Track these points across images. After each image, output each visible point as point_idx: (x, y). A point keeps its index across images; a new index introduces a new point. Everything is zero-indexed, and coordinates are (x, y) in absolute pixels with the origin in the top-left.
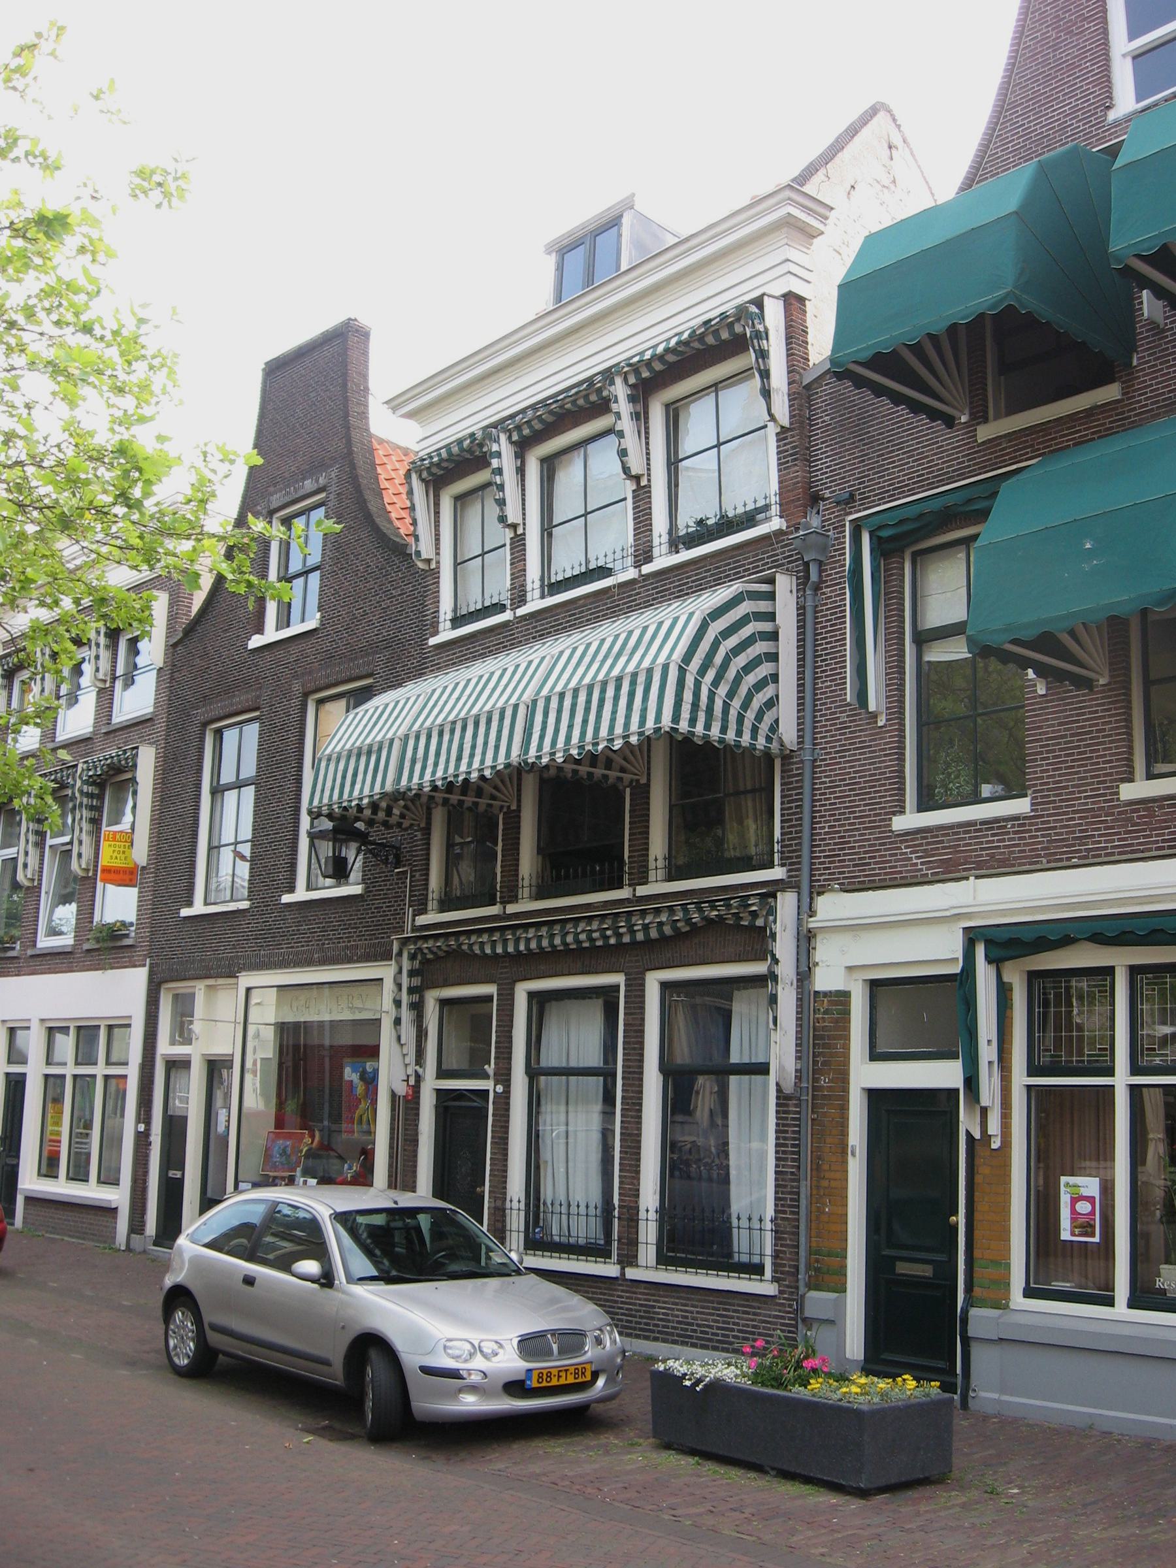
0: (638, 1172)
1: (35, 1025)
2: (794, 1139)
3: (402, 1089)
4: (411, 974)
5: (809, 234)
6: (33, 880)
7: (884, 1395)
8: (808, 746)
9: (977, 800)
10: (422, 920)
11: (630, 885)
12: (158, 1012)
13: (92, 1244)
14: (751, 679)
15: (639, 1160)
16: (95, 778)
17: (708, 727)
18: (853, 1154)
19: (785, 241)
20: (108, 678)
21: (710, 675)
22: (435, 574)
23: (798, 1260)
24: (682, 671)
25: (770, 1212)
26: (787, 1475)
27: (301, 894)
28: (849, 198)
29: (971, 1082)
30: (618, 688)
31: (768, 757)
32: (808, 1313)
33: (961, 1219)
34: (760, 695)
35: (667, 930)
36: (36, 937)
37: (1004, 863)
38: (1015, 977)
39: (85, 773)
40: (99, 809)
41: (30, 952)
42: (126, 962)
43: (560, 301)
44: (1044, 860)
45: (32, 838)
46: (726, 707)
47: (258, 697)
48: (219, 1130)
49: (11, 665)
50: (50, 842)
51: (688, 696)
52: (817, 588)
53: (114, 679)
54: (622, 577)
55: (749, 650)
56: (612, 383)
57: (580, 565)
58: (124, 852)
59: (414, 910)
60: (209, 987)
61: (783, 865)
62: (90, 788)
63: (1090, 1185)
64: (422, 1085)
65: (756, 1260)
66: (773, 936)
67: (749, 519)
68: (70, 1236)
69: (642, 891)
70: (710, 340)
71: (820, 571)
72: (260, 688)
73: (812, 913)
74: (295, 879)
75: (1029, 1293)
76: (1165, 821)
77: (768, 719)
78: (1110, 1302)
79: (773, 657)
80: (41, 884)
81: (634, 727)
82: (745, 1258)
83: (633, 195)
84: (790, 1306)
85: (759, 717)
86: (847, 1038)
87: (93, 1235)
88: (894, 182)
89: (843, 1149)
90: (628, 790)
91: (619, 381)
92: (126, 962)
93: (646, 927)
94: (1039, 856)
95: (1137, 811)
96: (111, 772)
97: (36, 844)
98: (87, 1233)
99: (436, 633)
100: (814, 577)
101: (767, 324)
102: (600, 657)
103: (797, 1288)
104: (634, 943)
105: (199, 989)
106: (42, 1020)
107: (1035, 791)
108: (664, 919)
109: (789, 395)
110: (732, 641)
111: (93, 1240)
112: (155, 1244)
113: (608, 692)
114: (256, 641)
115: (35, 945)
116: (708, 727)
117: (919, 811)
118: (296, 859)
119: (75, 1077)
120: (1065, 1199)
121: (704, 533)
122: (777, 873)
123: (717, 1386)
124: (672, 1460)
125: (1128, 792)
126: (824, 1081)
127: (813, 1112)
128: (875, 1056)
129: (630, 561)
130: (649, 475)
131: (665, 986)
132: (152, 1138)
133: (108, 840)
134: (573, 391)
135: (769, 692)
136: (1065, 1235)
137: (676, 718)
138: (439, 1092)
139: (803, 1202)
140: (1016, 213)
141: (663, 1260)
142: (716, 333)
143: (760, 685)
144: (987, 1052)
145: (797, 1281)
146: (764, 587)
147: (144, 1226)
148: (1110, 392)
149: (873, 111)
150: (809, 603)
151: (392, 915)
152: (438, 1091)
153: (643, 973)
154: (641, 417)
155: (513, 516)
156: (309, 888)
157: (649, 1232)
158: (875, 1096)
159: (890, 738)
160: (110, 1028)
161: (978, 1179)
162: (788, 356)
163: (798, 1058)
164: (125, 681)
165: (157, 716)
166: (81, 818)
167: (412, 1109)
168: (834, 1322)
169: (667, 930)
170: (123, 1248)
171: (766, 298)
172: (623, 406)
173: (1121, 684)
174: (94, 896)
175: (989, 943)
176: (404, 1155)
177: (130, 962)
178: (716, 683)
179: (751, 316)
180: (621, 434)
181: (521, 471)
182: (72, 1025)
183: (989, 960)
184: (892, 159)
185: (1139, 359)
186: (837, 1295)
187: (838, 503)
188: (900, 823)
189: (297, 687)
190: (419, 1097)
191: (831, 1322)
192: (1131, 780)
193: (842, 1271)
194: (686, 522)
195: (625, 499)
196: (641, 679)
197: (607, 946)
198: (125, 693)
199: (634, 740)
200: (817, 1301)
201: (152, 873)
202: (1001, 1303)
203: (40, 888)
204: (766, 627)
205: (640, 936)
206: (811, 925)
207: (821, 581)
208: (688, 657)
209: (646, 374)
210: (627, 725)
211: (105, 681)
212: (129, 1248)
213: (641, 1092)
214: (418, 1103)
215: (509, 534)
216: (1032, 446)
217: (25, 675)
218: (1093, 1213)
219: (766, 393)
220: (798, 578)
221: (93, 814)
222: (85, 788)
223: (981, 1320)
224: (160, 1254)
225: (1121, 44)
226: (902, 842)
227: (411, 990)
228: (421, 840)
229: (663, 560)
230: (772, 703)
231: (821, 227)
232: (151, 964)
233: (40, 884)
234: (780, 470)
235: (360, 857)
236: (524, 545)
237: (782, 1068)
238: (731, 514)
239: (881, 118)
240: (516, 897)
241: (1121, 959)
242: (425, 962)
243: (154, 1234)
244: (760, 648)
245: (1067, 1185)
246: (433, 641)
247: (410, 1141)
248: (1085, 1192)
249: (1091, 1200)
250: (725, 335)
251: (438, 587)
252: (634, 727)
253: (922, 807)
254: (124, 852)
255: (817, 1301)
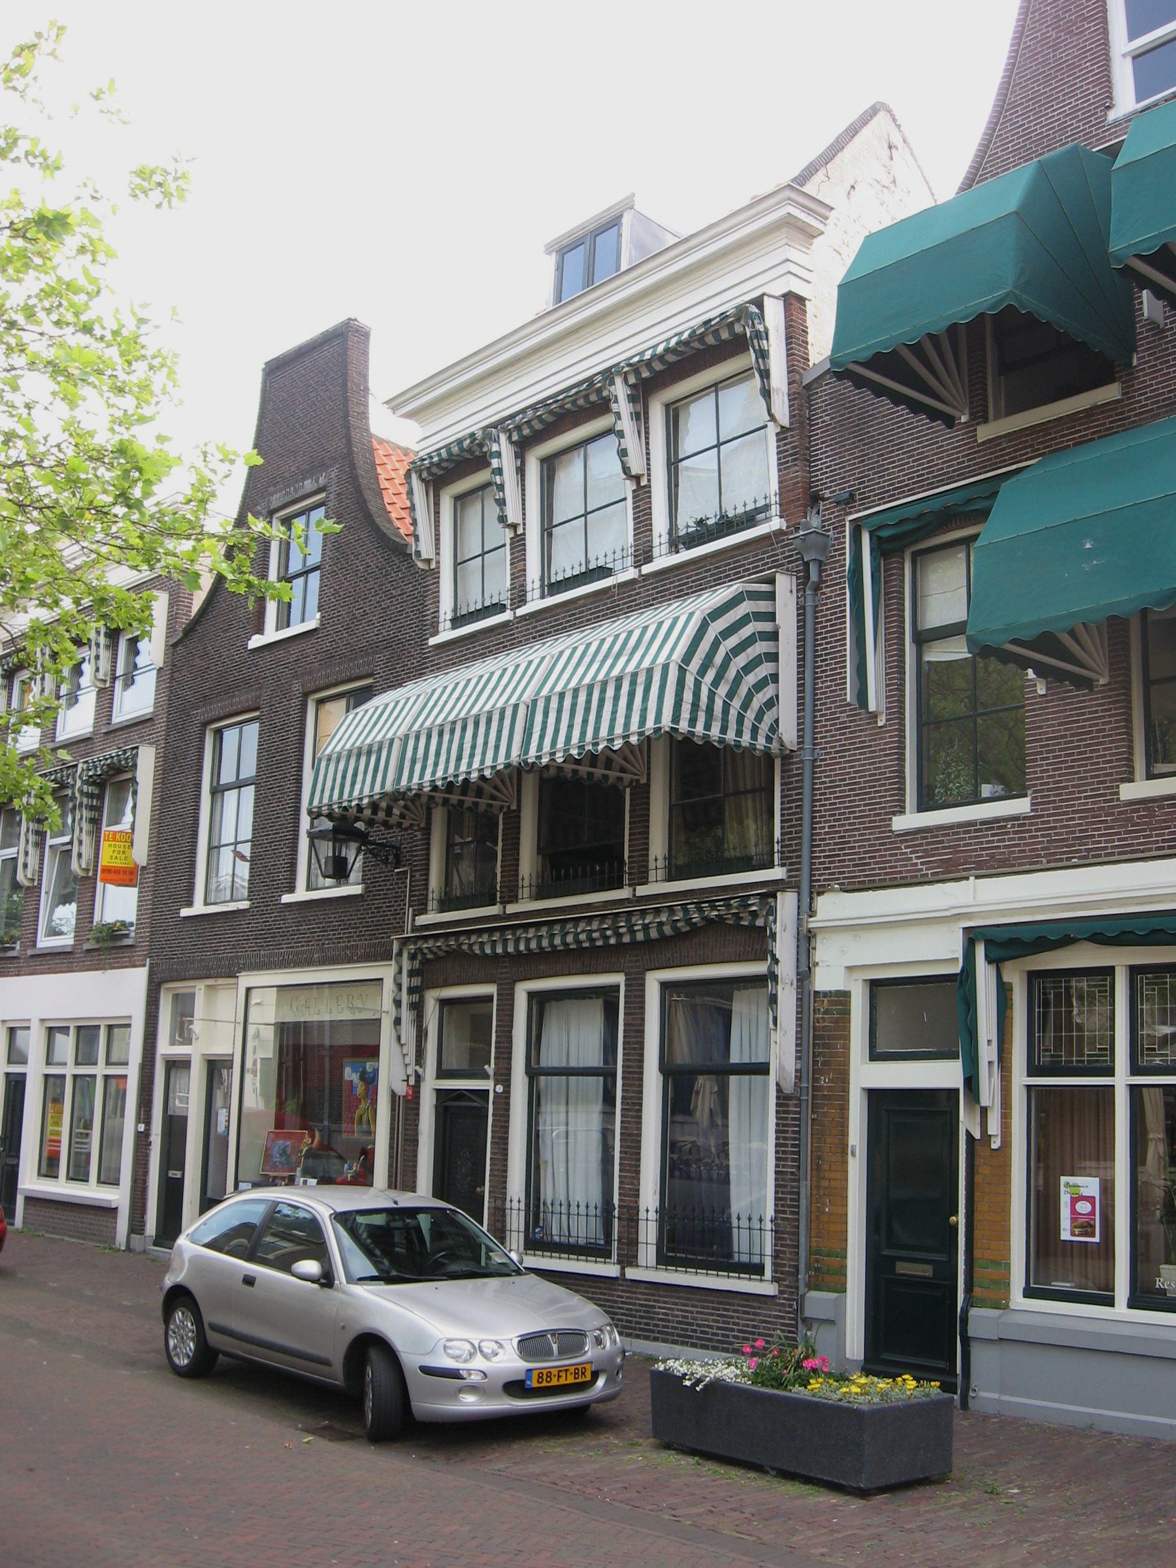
0: (638, 1172)
1: (35, 1025)
2: (794, 1139)
3: (402, 1089)
4: (411, 974)
5: (809, 234)
6: (33, 880)
7: (884, 1395)
8: (808, 746)
9: (977, 800)
10: (422, 920)
11: (630, 885)
12: (158, 1012)
13: (92, 1244)
14: (751, 679)
15: (639, 1160)
16: (95, 778)
17: (708, 727)
18: (853, 1154)
19: (785, 241)
20: (108, 678)
21: (710, 675)
22: (435, 574)
23: (798, 1260)
24: (682, 671)
25: (770, 1212)
26: (787, 1475)
27: (301, 894)
28: (849, 198)
29: (971, 1082)
30: (618, 688)
31: (768, 757)
32: (808, 1313)
33: (961, 1219)
34: (760, 695)
35: (667, 930)
36: (36, 937)
37: (1004, 863)
38: (1015, 977)
39: (85, 773)
40: (99, 809)
41: (30, 952)
42: (126, 962)
43: (560, 301)
44: (1044, 860)
45: (32, 838)
46: (726, 707)
47: (258, 697)
48: (219, 1130)
49: (11, 665)
50: (50, 842)
51: (688, 696)
52: (817, 588)
53: (114, 679)
54: (622, 577)
55: (749, 650)
56: (612, 383)
57: (580, 565)
58: (124, 852)
59: (414, 910)
60: (209, 987)
61: (783, 865)
62: (90, 788)
63: (1090, 1185)
64: (422, 1085)
65: (756, 1260)
66: (773, 936)
67: (749, 519)
68: (70, 1236)
69: (642, 891)
70: (710, 340)
71: (820, 571)
72: (260, 688)
73: (812, 913)
74: (295, 879)
75: (1029, 1293)
76: (1165, 821)
77: (768, 719)
78: (1110, 1302)
79: (773, 657)
80: (41, 884)
81: (634, 727)
82: (745, 1258)
83: (633, 195)
84: (790, 1306)
85: (759, 717)
86: (847, 1038)
87: (93, 1235)
88: (894, 182)
89: (843, 1149)
90: (628, 790)
91: (619, 381)
92: (126, 962)
93: (646, 927)
94: (1039, 856)
95: (1137, 811)
96: (111, 772)
97: (36, 844)
98: (87, 1233)
99: (436, 633)
100: (814, 577)
101: (767, 324)
102: (600, 657)
103: (797, 1288)
104: (634, 943)
105: (199, 989)
106: (42, 1020)
107: (1035, 791)
108: (664, 919)
109: (789, 395)
110: (732, 641)
111: (93, 1240)
112: (155, 1244)
113: (608, 692)
114: (256, 641)
115: (35, 945)
116: (708, 727)
117: (919, 811)
118: (296, 859)
119: (75, 1077)
120: (1065, 1199)
121: (704, 533)
122: (777, 873)
123: (717, 1386)
124: (672, 1460)
125: (1128, 792)
126: (824, 1081)
127: (813, 1112)
128: (875, 1056)
129: (630, 561)
130: (649, 475)
131: (665, 986)
132: (152, 1138)
133: (108, 840)
134: (573, 391)
135: (769, 692)
136: (1065, 1235)
137: (676, 718)
138: (439, 1092)
139: (803, 1202)
140: (1016, 213)
141: (663, 1260)
142: (716, 333)
143: (760, 685)
144: (987, 1052)
145: (797, 1281)
146: (764, 587)
147: (144, 1226)
148: (1110, 392)
149: (873, 111)
150: (809, 603)
151: (392, 915)
152: (438, 1091)
153: (643, 973)
154: (641, 417)
155: (513, 516)
156: (309, 888)
157: (649, 1232)
158: (875, 1096)
159: (890, 738)
160: (110, 1028)
161: (978, 1179)
162: (788, 356)
163: (798, 1058)
164: (125, 681)
165: (157, 716)
166: (81, 818)
167: (412, 1109)
168: (834, 1322)
169: (667, 930)
170: (123, 1248)
171: (766, 298)
172: (623, 406)
173: (1121, 684)
174: (94, 896)
175: (989, 943)
176: (404, 1155)
177: (130, 962)
178: (716, 683)
179: (751, 316)
180: (621, 434)
181: (521, 471)
182: (72, 1025)
183: (989, 960)
184: (892, 159)
185: (1139, 359)
186: (837, 1295)
187: (838, 503)
188: (900, 823)
189: (297, 687)
190: (419, 1097)
191: (831, 1322)
192: (1131, 780)
193: (842, 1271)
194: (686, 522)
195: (625, 499)
196: (641, 679)
197: (607, 946)
198: (125, 693)
199: (634, 740)
200: (817, 1301)
201: (152, 873)
202: (1001, 1303)
203: (40, 888)
204: (766, 627)
205: (640, 936)
206: (811, 925)
207: (821, 581)
208: (688, 657)
209: (646, 374)
210: (627, 725)
211: (105, 681)
212: (129, 1248)
213: (641, 1092)
214: (418, 1103)
215: (509, 534)
216: (1032, 446)
217: (25, 675)
218: (1093, 1213)
219: (766, 393)
220: (798, 578)
221: (93, 814)
222: (85, 788)
223: (981, 1320)
224: (160, 1254)
225: (1121, 44)
226: (902, 842)
227: (411, 990)
228: (421, 840)
229: (663, 560)
230: (772, 703)
231: (821, 227)
232: (151, 964)
233: (40, 884)
234: (780, 470)
235: (360, 857)
236: (524, 545)
237: (782, 1068)
238: (731, 514)
239: (881, 118)
240: (516, 897)
241: (1121, 959)
242: (425, 962)
243: (154, 1234)
244: (760, 648)
245: (1067, 1185)
246: (433, 641)
247: (410, 1141)
248: (1085, 1192)
249: (1091, 1200)
250: (725, 335)
251: (438, 587)
252: (634, 727)
253: (922, 807)
254: (124, 852)
255: (817, 1301)
